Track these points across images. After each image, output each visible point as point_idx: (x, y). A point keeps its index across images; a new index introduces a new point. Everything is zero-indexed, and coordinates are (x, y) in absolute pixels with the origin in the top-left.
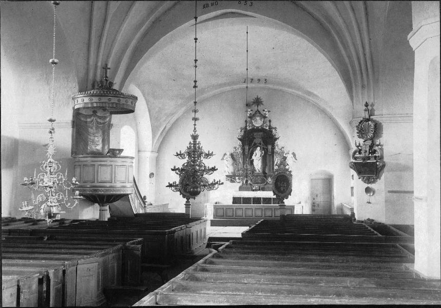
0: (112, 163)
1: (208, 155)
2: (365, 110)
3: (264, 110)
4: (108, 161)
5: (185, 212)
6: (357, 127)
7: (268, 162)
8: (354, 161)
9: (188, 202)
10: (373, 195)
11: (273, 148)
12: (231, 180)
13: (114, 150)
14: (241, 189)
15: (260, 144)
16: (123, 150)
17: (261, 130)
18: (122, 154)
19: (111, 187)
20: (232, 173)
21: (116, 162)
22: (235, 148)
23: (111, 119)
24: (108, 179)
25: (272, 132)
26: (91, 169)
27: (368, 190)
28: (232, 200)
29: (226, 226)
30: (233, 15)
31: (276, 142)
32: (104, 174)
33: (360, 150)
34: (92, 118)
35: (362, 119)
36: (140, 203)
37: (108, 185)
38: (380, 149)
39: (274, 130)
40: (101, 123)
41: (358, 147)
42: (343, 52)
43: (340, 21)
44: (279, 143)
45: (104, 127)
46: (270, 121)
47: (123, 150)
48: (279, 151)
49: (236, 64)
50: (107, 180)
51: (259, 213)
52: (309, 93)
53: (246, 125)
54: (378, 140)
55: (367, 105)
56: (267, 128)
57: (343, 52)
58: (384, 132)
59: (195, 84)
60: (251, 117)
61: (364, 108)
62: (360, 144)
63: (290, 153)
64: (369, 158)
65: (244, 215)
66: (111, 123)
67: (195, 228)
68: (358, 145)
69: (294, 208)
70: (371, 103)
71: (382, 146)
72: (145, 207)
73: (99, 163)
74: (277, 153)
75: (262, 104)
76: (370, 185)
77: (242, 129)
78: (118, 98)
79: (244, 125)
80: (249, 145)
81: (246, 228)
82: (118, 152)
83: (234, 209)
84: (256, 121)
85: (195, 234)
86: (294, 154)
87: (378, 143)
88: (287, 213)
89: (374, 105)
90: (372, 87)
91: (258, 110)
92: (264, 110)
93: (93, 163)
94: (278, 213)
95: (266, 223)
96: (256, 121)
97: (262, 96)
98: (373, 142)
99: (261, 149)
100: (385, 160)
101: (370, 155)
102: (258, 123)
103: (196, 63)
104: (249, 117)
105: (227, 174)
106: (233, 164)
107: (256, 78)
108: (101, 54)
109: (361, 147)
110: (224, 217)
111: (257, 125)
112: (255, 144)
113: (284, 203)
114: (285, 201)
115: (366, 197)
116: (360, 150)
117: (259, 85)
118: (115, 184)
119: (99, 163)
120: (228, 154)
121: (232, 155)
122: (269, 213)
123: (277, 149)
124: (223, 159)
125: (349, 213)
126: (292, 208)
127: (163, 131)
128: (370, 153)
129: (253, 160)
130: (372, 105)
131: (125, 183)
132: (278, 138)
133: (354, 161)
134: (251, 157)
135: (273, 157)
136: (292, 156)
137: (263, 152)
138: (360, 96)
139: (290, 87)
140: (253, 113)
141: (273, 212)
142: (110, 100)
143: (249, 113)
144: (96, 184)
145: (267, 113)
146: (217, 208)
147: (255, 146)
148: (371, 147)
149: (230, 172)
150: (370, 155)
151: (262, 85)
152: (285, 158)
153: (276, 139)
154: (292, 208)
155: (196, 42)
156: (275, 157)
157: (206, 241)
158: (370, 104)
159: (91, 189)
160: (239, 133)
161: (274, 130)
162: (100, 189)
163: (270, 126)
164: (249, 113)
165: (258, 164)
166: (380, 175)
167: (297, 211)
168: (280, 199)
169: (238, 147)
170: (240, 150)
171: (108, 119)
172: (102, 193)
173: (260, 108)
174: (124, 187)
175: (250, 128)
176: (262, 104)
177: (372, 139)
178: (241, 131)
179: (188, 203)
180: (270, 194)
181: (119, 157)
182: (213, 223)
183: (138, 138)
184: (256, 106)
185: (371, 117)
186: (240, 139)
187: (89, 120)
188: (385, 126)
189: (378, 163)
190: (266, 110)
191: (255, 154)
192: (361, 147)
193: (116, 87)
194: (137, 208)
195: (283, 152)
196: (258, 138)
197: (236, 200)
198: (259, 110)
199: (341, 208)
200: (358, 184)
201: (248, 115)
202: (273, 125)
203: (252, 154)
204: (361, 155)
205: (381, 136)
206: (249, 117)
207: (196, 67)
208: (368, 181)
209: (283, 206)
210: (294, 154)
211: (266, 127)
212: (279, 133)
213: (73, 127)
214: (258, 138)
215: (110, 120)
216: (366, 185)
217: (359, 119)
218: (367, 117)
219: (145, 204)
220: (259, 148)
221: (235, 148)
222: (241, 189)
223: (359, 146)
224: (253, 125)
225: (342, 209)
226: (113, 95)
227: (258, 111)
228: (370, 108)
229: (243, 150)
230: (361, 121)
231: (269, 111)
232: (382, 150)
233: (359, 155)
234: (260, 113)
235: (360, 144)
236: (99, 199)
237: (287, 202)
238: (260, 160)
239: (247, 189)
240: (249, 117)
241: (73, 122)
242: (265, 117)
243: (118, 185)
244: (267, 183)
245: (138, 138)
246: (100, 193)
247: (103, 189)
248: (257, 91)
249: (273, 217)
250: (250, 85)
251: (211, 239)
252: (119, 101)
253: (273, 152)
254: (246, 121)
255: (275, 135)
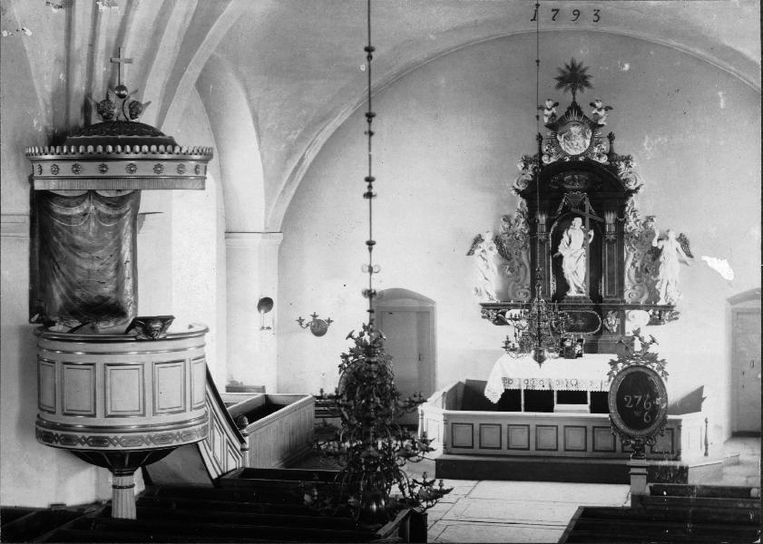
0: (143, 358)
3: (592, 105)
7: (606, 258)
11: (620, 223)
12: (498, 318)
13: (148, 320)
16: (171, 318)
17: (582, 165)
18: (173, 329)
25: (616, 170)
26: (84, 375)
29: (480, 479)
31: (629, 203)
34: (85, 206)
36: (230, 443)
39: (623, 165)
40: (109, 218)
46: (611, 137)
47: (171, 318)
53: (540, 149)
56: (604, 160)
59: (370, 187)
60: (556, 125)
63: (673, 236)
65: (533, 447)
69: (679, 428)
72: (243, 450)
73: (108, 359)
74: (631, 235)
77: (527, 161)
78: (156, 163)
79: (536, 152)
80: (550, 211)
82: (158, 325)
86: (683, 241)
91: (574, 103)
99: (584, 224)
102: (576, 144)
103: (370, 122)
104: (548, 126)
105: (486, 300)
106: (501, 268)
111: (572, 152)
119: (108, 359)
120: (488, 238)
121: (497, 240)
123: (632, 225)
124: (471, 253)
127: (296, 169)
129: (561, 257)
131: (184, 411)
132: (636, 191)
134: (555, 249)
136: (678, 245)
137: (592, 233)
140: (560, 112)
142: (131, 169)
143: (549, 113)
145: (602, 113)
147: (566, 221)
152: (657, 253)
155: (370, 57)
156: (626, 248)
159: (87, 435)
160: (518, 174)
161: (623, 165)
163: (610, 154)
164: (546, 112)
169: (515, 215)
170: (521, 226)
173: (582, 97)
175: (553, 160)
178: (526, 167)
181: (164, 339)
184: (570, 92)
186: (522, 194)
187: (77, 211)
190: (599, 105)
191: (566, 238)
193: (148, 118)
195: (651, 234)
203: (557, 239)
206: (549, 126)
207: (371, 134)
210: (683, 241)
211: (599, 156)
219: (242, 441)
220: (578, 221)
221: (507, 219)
224: (560, 151)
226: (139, 156)
227: (575, 107)
229: (531, 222)
231: (607, 108)
234: (580, 113)
236: (110, 460)
238: (583, 258)
240: (549, 126)
242: (595, 126)
244: (603, 328)
246: (111, 447)
253: (621, 233)
254: (540, 138)
255: (626, 181)
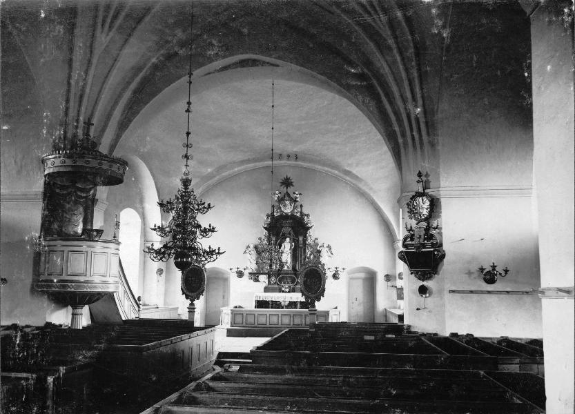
0: (88, 249)
1: (205, 232)
2: (418, 182)
3: (294, 193)
4: (85, 245)
5: (187, 319)
6: (408, 204)
8: (404, 250)
9: (192, 304)
10: (429, 296)
11: (305, 241)
14: (266, 290)
15: (290, 234)
17: (292, 217)
19: (86, 282)
20: (256, 270)
21: (93, 247)
22: (260, 239)
23: (96, 190)
24: (81, 271)
25: (303, 219)
27: (423, 290)
28: (254, 304)
30: (254, 63)
31: (308, 232)
32: (77, 264)
33: (413, 235)
34: (70, 190)
35: (414, 194)
37: (82, 279)
38: (439, 233)
41: (409, 231)
42: (388, 107)
43: (385, 70)
44: (313, 234)
45: (86, 202)
46: (301, 206)
48: (312, 243)
49: (261, 135)
50: (80, 272)
51: (286, 320)
52: (348, 173)
54: (436, 222)
55: (420, 175)
56: (298, 215)
57: (388, 107)
58: (442, 210)
60: (281, 200)
61: (418, 178)
62: (411, 227)
63: (325, 245)
64: (424, 246)
66: (96, 197)
67: (195, 341)
68: (409, 228)
70: (425, 173)
71: (441, 228)
75: (293, 186)
76: (425, 283)
77: (268, 216)
81: (261, 341)
83: (268, 315)
84: (285, 206)
85: (195, 350)
86: (329, 247)
87: (435, 225)
88: (321, 320)
89: (429, 176)
90: (426, 154)
91: (287, 192)
92: (294, 193)
93: (62, 249)
94: (308, 321)
95: (294, 333)
96: (285, 206)
97: (291, 174)
98: (428, 223)
100: (445, 247)
101: (426, 242)
102: (288, 210)
105: (251, 271)
107: (285, 154)
108: (83, 109)
109: (413, 231)
110: (303, 326)
111: (286, 211)
112: (284, 234)
113: (314, 306)
114: (317, 303)
115: (421, 300)
116: (413, 235)
117: (290, 162)
118: (90, 279)
120: (252, 246)
121: (256, 247)
122: (297, 321)
123: (309, 241)
124: (245, 252)
125: (396, 321)
126: (326, 314)
128: (425, 239)
130: (427, 175)
133: (404, 250)
135: (305, 250)
138: (411, 161)
139: (324, 165)
141: (301, 319)
144: (64, 277)
146: (237, 313)
148: (427, 229)
149: (253, 268)
150: (426, 242)
151: (292, 162)
153: (309, 228)
154: (326, 314)
156: (307, 250)
157: (214, 358)
158: (424, 173)
160: (263, 220)
162: (69, 284)
163: (301, 212)
165: (287, 257)
166: (438, 270)
167: (333, 319)
168: (308, 304)
171: (92, 192)
172: (73, 290)
173: (290, 190)
174: (105, 282)
175: (278, 214)
176: (293, 186)
177: (428, 219)
178: (268, 218)
179: (192, 310)
180: (298, 297)
182: (230, 333)
183: (144, 225)
185: (426, 191)
186: (265, 228)
188: (444, 202)
189: (436, 253)
190: (297, 193)
192: (413, 231)
194: (127, 311)
195: (317, 245)
196: (287, 227)
197: (261, 304)
198: (289, 192)
199: (386, 314)
200: (409, 282)
201: (276, 198)
202: (305, 211)
204: (413, 242)
205: (439, 216)
208: (424, 276)
209: (314, 312)
212: (312, 221)
213: (44, 200)
214: (287, 227)
215: (94, 195)
216: (421, 283)
217: (411, 193)
218: (421, 190)
219: (139, 307)
220: (288, 239)
221: (260, 239)
222: (266, 290)
223: (411, 229)
225: (386, 316)
227: (287, 194)
228: (424, 178)
230: (414, 197)
231: (300, 194)
232: (440, 234)
233: (410, 242)
235: (411, 227)
237: (320, 306)
239: (273, 290)
241: (45, 194)
243: (97, 279)
245: (144, 225)
247: (73, 284)
248: (286, 168)
249: (268, 325)
250: (276, 162)
251: (221, 355)
252: (100, 164)
254: (273, 206)
